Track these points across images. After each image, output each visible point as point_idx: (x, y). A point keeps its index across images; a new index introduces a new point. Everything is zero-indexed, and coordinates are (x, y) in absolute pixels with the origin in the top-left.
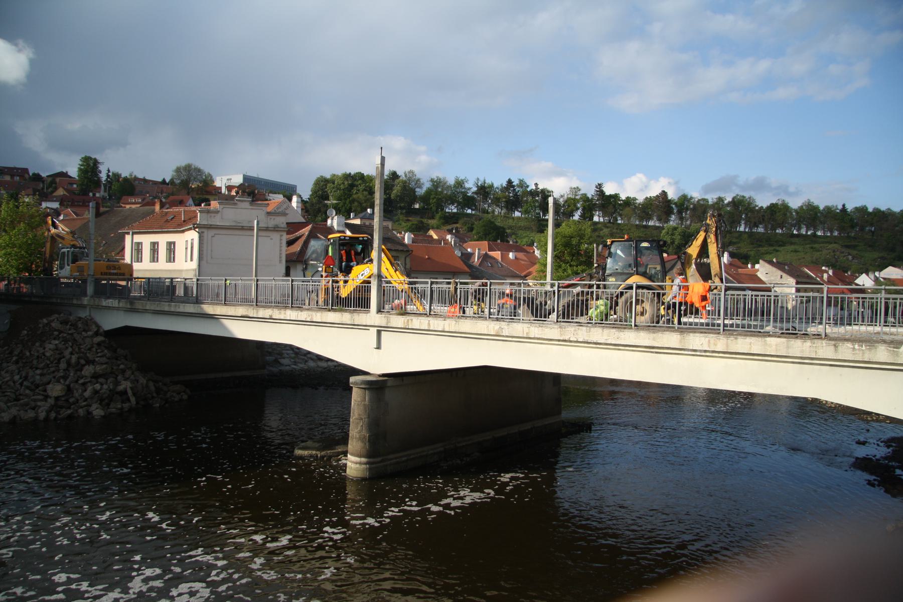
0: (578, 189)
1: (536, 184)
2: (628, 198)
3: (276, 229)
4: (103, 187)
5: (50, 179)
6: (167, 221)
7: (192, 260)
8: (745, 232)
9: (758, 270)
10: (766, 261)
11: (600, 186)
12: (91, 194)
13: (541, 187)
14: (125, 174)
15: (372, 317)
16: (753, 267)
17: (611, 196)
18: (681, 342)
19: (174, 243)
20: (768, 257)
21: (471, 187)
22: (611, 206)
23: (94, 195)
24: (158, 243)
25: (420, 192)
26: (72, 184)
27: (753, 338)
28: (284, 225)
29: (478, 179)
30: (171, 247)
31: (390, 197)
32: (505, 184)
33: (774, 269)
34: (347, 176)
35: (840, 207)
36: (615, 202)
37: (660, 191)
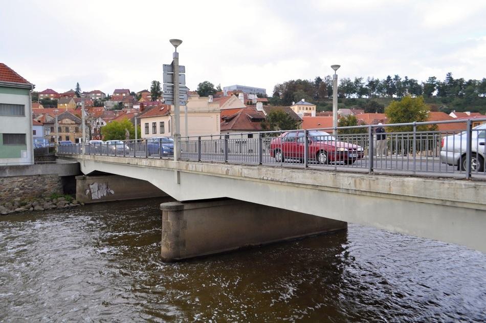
1: (406, 77)
3: (214, 111)
5: (139, 94)
13: (409, 78)
15: (173, 163)
18: (334, 181)
21: (365, 83)
29: (369, 78)
32: (386, 79)
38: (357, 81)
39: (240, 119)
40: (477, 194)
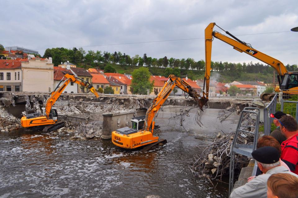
1: (124, 54)
2: (154, 59)
3: (50, 69)
8: (191, 70)
11: (145, 55)
13: (126, 54)
17: (149, 58)
19: (10, 73)
25: (84, 55)
30: (9, 75)
32: (114, 53)
35: (220, 62)
38: (98, 53)
39: (59, 74)
40: (210, 88)
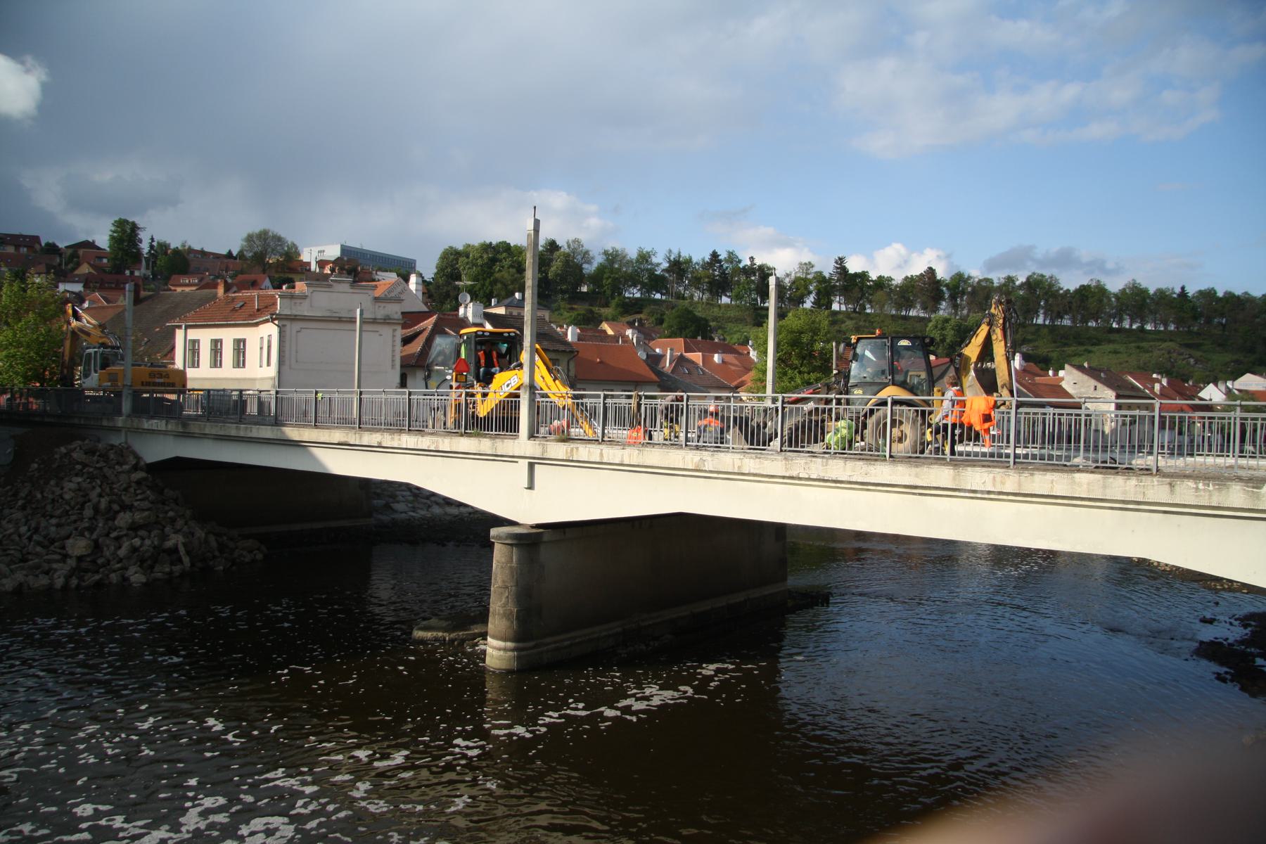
0: (810, 265)
1: (752, 259)
2: (880, 277)
3: (387, 321)
4: (144, 262)
5: (70, 251)
6: (234, 310)
7: (269, 364)
8: (1044, 325)
9: (1062, 379)
10: (1073, 366)
11: (841, 261)
12: (127, 272)
13: (758, 262)
14: (175, 244)
16: (1056, 374)
17: (856, 275)
19: (244, 341)
20: (1076, 361)
21: (661, 261)
22: (857, 289)
23: (132, 273)
24: (221, 341)
25: (589, 269)
26: (101, 258)
27: (1056, 474)
28: (399, 316)
29: (670, 251)
30: (240, 346)
31: (546, 277)
32: (707, 258)
33: (1085, 377)
34: (487, 247)
35: (1178, 290)
36: (863, 283)
37: (925, 268)
